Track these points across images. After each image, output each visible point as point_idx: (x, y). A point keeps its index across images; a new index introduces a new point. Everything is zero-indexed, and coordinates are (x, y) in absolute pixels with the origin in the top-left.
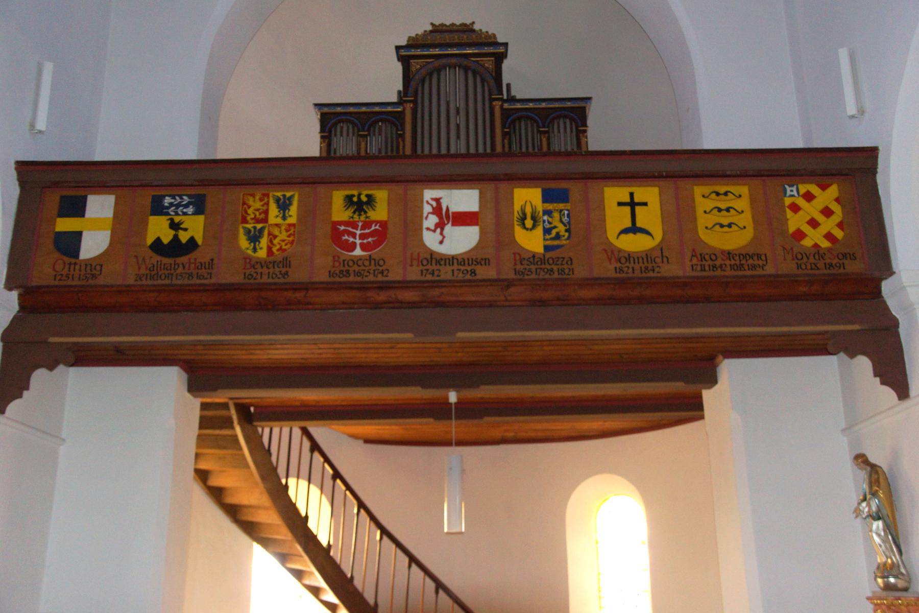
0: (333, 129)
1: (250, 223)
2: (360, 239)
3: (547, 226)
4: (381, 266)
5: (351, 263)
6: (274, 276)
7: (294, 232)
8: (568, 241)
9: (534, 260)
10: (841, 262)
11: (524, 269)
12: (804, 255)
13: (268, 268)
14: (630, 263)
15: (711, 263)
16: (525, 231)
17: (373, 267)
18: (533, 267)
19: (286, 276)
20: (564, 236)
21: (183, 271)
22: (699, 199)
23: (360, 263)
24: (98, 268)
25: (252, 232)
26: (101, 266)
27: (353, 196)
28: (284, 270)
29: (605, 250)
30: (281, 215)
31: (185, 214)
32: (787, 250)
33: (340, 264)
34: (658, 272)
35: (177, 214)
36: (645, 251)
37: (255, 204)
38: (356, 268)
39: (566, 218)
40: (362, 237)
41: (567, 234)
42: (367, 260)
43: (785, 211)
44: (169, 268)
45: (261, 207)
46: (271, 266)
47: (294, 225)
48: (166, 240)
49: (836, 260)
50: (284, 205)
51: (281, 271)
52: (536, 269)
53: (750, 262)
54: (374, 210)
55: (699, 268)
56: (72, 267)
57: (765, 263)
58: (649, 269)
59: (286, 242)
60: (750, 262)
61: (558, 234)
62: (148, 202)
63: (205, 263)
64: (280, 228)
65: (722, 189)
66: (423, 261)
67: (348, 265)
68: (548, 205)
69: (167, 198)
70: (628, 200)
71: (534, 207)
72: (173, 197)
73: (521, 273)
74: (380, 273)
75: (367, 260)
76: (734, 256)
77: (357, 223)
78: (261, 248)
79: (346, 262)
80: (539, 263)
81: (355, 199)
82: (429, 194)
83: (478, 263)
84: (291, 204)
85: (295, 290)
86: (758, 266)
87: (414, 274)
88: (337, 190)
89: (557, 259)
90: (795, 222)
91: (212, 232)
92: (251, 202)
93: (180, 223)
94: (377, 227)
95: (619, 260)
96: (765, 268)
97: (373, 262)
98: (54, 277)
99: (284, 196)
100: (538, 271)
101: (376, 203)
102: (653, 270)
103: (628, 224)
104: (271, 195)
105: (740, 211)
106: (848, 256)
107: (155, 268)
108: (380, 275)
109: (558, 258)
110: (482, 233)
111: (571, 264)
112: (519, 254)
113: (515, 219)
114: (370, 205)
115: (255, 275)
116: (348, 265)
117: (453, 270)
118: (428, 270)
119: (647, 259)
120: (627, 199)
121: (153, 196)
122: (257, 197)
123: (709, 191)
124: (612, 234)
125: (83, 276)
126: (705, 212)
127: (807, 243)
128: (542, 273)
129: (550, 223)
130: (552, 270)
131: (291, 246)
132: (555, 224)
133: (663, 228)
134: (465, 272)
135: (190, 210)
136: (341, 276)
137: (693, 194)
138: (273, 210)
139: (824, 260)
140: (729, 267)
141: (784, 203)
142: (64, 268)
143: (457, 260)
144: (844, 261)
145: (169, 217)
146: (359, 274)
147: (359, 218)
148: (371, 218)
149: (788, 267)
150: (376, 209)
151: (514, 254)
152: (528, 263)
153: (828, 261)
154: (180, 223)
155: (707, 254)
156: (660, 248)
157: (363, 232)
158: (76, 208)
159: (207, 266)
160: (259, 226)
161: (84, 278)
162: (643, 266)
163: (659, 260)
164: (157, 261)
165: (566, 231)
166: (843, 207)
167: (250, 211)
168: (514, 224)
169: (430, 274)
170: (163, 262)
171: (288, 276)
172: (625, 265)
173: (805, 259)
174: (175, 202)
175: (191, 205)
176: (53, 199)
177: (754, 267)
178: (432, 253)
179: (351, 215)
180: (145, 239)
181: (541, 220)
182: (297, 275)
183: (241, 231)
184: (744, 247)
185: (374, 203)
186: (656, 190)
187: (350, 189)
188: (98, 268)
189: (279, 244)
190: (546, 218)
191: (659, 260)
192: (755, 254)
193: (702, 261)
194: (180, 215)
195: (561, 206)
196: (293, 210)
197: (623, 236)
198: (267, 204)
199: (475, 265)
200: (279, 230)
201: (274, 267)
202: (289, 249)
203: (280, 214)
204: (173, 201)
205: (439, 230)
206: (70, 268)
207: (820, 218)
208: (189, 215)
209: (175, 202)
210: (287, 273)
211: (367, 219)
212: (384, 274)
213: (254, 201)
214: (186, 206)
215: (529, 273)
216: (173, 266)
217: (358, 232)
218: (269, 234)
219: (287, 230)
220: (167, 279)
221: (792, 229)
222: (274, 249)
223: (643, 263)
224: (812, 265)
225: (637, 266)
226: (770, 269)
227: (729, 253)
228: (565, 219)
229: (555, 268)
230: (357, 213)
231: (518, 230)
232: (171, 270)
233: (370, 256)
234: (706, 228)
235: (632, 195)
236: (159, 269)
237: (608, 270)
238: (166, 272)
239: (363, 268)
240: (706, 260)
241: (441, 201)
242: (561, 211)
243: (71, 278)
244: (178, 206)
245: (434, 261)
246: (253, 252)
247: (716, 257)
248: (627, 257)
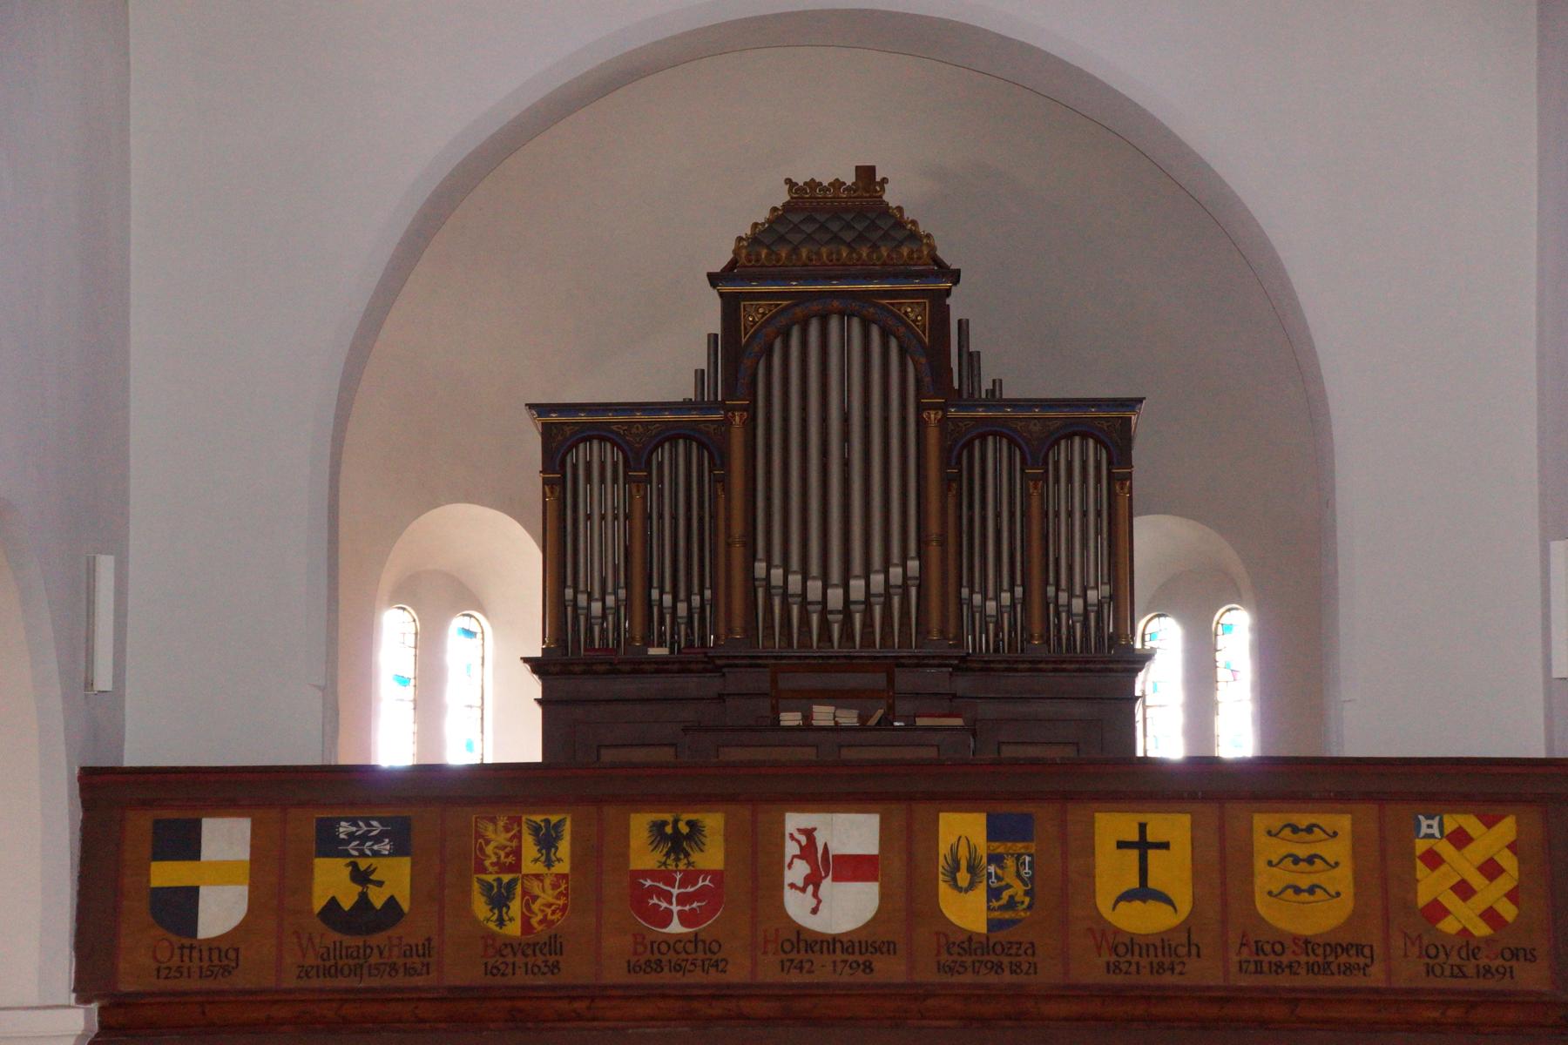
1: (491, 873)
2: (678, 904)
3: (994, 883)
4: (714, 953)
5: (664, 948)
6: (536, 970)
7: (566, 889)
8: (1028, 913)
9: (970, 944)
10: (1507, 964)
11: (953, 962)
12: (1441, 949)
13: (524, 954)
14: (1133, 954)
15: (1273, 958)
16: (956, 892)
17: (700, 955)
18: (968, 959)
19: (556, 971)
20: (1023, 903)
21: (381, 961)
22: (1260, 840)
23: (679, 946)
24: (232, 954)
25: (495, 890)
26: (237, 950)
27: (664, 823)
28: (552, 959)
29: (1090, 930)
30: (543, 859)
31: (376, 854)
32: (1410, 938)
33: (646, 947)
34: (1181, 973)
35: (363, 855)
36: (1160, 933)
37: (497, 837)
38: (672, 955)
39: (1027, 870)
40: (682, 900)
41: (1027, 900)
42: (690, 941)
43: (1414, 868)
44: (355, 954)
45: (509, 843)
46: (530, 952)
47: (564, 876)
48: (347, 904)
49: (1500, 962)
50: (547, 842)
51: (546, 962)
52: (974, 963)
53: (1343, 958)
54: (702, 851)
55: (1252, 967)
56: (186, 952)
57: (1368, 961)
58: (1166, 967)
59: (553, 907)
60: (1343, 958)
61: (1011, 897)
62: (310, 831)
63: (417, 946)
64: (542, 881)
65: (1304, 820)
66: (1119, 946)
67: (659, 951)
68: (997, 844)
69: (343, 824)
70: (1135, 837)
71: (972, 847)
72: (354, 823)
73: (947, 969)
74: (713, 966)
75: (690, 941)
76: (1316, 946)
77: (674, 874)
78: (511, 919)
79: (655, 946)
80: (979, 951)
81: (669, 830)
82: (795, 821)
83: (878, 950)
84: (559, 837)
85: (573, 999)
86: (1356, 966)
87: (770, 972)
88: (638, 812)
89: (1009, 946)
90: (1430, 886)
91: (431, 889)
92: (490, 834)
93: (370, 871)
94: (707, 882)
95: (1114, 949)
96: (1369, 970)
97: (700, 946)
98: (155, 973)
99: (547, 821)
100: (977, 964)
101: (705, 837)
102: (1173, 970)
103: (1134, 883)
104: (524, 819)
105: (1332, 863)
106: (1521, 954)
107: (332, 954)
108: (712, 970)
109: (1010, 943)
110: (884, 896)
111: (1034, 954)
112: (946, 936)
113: (940, 869)
114: (661, 838)
115: (502, 967)
116: (659, 951)
117: (834, 962)
118: (792, 961)
119: (1163, 948)
120: (1134, 836)
121: (320, 820)
122: (501, 824)
123: (1279, 824)
124: (1104, 904)
125: (207, 970)
126: (1270, 863)
127: (1449, 926)
128: (983, 971)
129: (999, 878)
130: (1000, 965)
131: (562, 916)
132: (1008, 880)
133: (1193, 893)
134: (854, 965)
135: (385, 847)
136: (648, 970)
137: (1250, 830)
138: (530, 849)
139: (1476, 959)
140: (1305, 967)
141: (1413, 848)
142: (172, 957)
143: (841, 942)
144: (1514, 963)
145: (348, 860)
146: (678, 968)
147: (677, 866)
148: (695, 864)
149: (1409, 973)
150: (706, 848)
151: (937, 934)
152: (961, 951)
153: (1483, 962)
154: (370, 871)
155: (1268, 942)
156: (1187, 927)
157: (682, 890)
158: (186, 845)
159: (421, 952)
160: (506, 878)
161: (209, 973)
162: (1155, 961)
163: (1183, 951)
164: (334, 942)
165: (1027, 893)
166: (1521, 862)
167: (489, 849)
168: (937, 879)
169: (795, 967)
170: (344, 944)
171: (559, 969)
172: (1125, 959)
173: (1442, 955)
174: (357, 831)
175: (386, 838)
176: (140, 824)
177: (1348, 969)
178: (800, 931)
179: (663, 859)
180: (310, 902)
181: (985, 872)
182: (576, 969)
183: (476, 886)
184: (1334, 931)
185: (701, 837)
186: (1186, 819)
187: (660, 811)
188: (232, 954)
189: (543, 911)
190: (992, 869)
191: (1183, 951)
192: (1352, 945)
193: (1258, 954)
194: (368, 856)
195: (1019, 847)
196: (564, 848)
197: (1123, 905)
198: (518, 836)
199: (871, 953)
200: (541, 884)
201: (535, 955)
202: (558, 920)
203: (542, 855)
204: (354, 829)
205: (810, 888)
206: (182, 956)
207: (1477, 880)
208: (384, 856)
209: (357, 831)
210: (556, 965)
211: (691, 868)
212: (720, 969)
213: (495, 831)
214: (378, 839)
215: (961, 970)
216: (361, 951)
217: (675, 891)
218: (525, 893)
219: (555, 886)
220: (352, 975)
221: (1423, 899)
222: (534, 921)
223: (1156, 956)
224: (1455, 968)
225: (1144, 962)
226: (1376, 976)
227: (1307, 942)
228: (1027, 871)
229: (1006, 960)
230: (672, 857)
231: (943, 888)
232: (358, 957)
233: (696, 934)
234: (1270, 893)
235: (1143, 827)
236: (338, 958)
237: (1092, 969)
238: (351, 962)
239: (684, 956)
240: (1266, 955)
241: (816, 834)
242: (1019, 856)
243: (185, 974)
244: (364, 838)
245: (802, 945)
246: (497, 926)
247: (1283, 948)
248: (1128, 943)
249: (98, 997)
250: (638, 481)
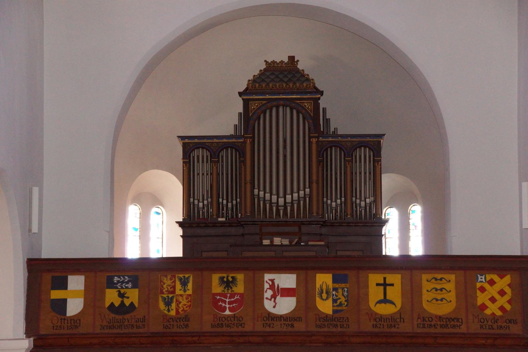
0: (325, 153)
1: (165, 294)
2: (228, 305)
3: (335, 297)
4: (240, 321)
5: (224, 319)
6: (180, 327)
7: (191, 299)
8: (346, 308)
9: (327, 318)
10: (508, 325)
11: (321, 324)
12: (485, 320)
13: (176, 321)
14: (381, 321)
15: (429, 323)
16: (322, 301)
17: (236, 322)
18: (326, 323)
19: (187, 327)
20: (344, 304)
21: (128, 324)
22: (424, 283)
23: (229, 319)
24: (78, 322)
25: (167, 300)
26: (80, 320)
27: (224, 277)
28: (186, 323)
29: (367, 313)
30: (183, 289)
31: (127, 288)
32: (475, 316)
33: (217, 319)
34: (398, 328)
35: (122, 288)
36: (391, 314)
37: (167, 282)
38: (226, 322)
39: (346, 293)
40: (230, 303)
41: (346, 303)
42: (232, 317)
43: (476, 292)
44: (120, 321)
45: (171, 284)
47: (190, 295)
48: (117, 304)
49: (505, 324)
50: (184, 283)
51: (184, 324)
52: (328, 324)
53: (452, 323)
54: (236, 287)
55: (422, 326)
56: (63, 321)
57: (461, 324)
58: (393, 326)
59: (186, 306)
60: (452, 323)
61: (341, 302)
62: (104, 280)
63: (140, 319)
64: (182, 297)
65: (439, 276)
67: (222, 320)
68: (336, 284)
69: (115, 277)
70: (382, 282)
71: (327, 285)
72: (119, 277)
73: (319, 326)
74: (240, 325)
75: (232, 317)
76: (443, 319)
77: (227, 294)
78: (172, 310)
79: (221, 319)
80: (330, 321)
81: (225, 279)
82: (268, 277)
83: (296, 320)
84: (188, 282)
85: (193, 336)
86: (457, 325)
87: (259, 327)
88: (215, 274)
89: (340, 319)
90: (482, 298)
91: (145, 299)
92: (165, 281)
93: (125, 293)
94: (238, 297)
95: (375, 320)
96: (461, 327)
97: (236, 319)
99: (184, 277)
100: (329, 325)
101: (238, 282)
102: (395, 327)
103: (382, 297)
104: (176, 276)
105: (449, 291)
106: (512, 321)
107: (112, 321)
108: (240, 327)
109: (340, 318)
110: (298, 302)
111: (348, 321)
112: (319, 315)
113: (317, 293)
115: (169, 326)
116: (222, 320)
117: (281, 324)
118: (267, 324)
119: (392, 319)
120: (382, 282)
121: (108, 276)
122: (169, 277)
123: (431, 278)
124: (372, 304)
125: (70, 327)
126: (428, 291)
127: (488, 312)
129: (336, 296)
130: (337, 325)
131: (189, 308)
132: (339, 296)
133: (402, 301)
134: (288, 325)
135: (130, 285)
136: (218, 327)
137: (421, 280)
138: (178, 286)
139: (497, 323)
140: (439, 326)
141: (476, 286)
142: (58, 322)
143: (283, 317)
144: (510, 324)
145: (117, 290)
146: (228, 326)
147: (228, 292)
148: (234, 291)
149: (475, 328)
150: (238, 286)
151: (316, 314)
152: (324, 320)
153: (499, 324)
154: (125, 293)
155: (427, 317)
156: (400, 312)
157: (230, 300)
158: (63, 285)
159: (142, 321)
160: (170, 296)
161: (70, 328)
162: (389, 324)
163: (398, 320)
164: (113, 317)
165: (346, 301)
166: (512, 290)
167: (165, 286)
168: (315, 296)
169: (268, 326)
170: (116, 318)
171: (188, 327)
172: (379, 323)
173: (486, 322)
174: (120, 280)
175: (130, 282)
176: (47, 278)
177: (454, 326)
178: (269, 313)
179: (223, 289)
180: (104, 304)
181: (332, 294)
182: (194, 327)
183: (160, 298)
184: (449, 314)
185: (236, 282)
186: (399, 276)
187: (222, 273)
188: (78, 322)
189: (183, 307)
190: (334, 293)
191: (398, 320)
192: (455, 318)
193: (423, 321)
194: (124, 288)
195: (343, 285)
196: (190, 286)
197: (378, 305)
198: (175, 282)
199: (293, 321)
200: (182, 298)
201: (180, 322)
202: (188, 310)
203: (183, 288)
204: (119, 279)
205: (273, 299)
206: (61, 322)
207: (497, 297)
208: (129, 288)
209: (120, 280)
210: (187, 325)
211: (233, 292)
212: (242, 326)
213: (167, 280)
214: (127, 283)
215: (324, 327)
216: (122, 320)
217: (227, 300)
218: (177, 301)
219: (187, 299)
220: (119, 329)
221: (479, 303)
222: (180, 310)
223: (389, 322)
224: (490, 326)
225: (385, 324)
226: (463, 329)
227: (440, 317)
228: (346, 293)
229: (339, 323)
230: (226, 289)
231: (318, 299)
232: (121, 322)
233: (234, 315)
234: (428, 301)
235: (385, 279)
236: (114, 323)
237: (368, 326)
238: (118, 324)
239: (230, 322)
240: (426, 322)
241: (275, 281)
242: (343, 288)
243: (62, 328)
244: (123, 282)
245: (270, 318)
246: (167, 312)
247: (432, 319)
248: (380, 318)
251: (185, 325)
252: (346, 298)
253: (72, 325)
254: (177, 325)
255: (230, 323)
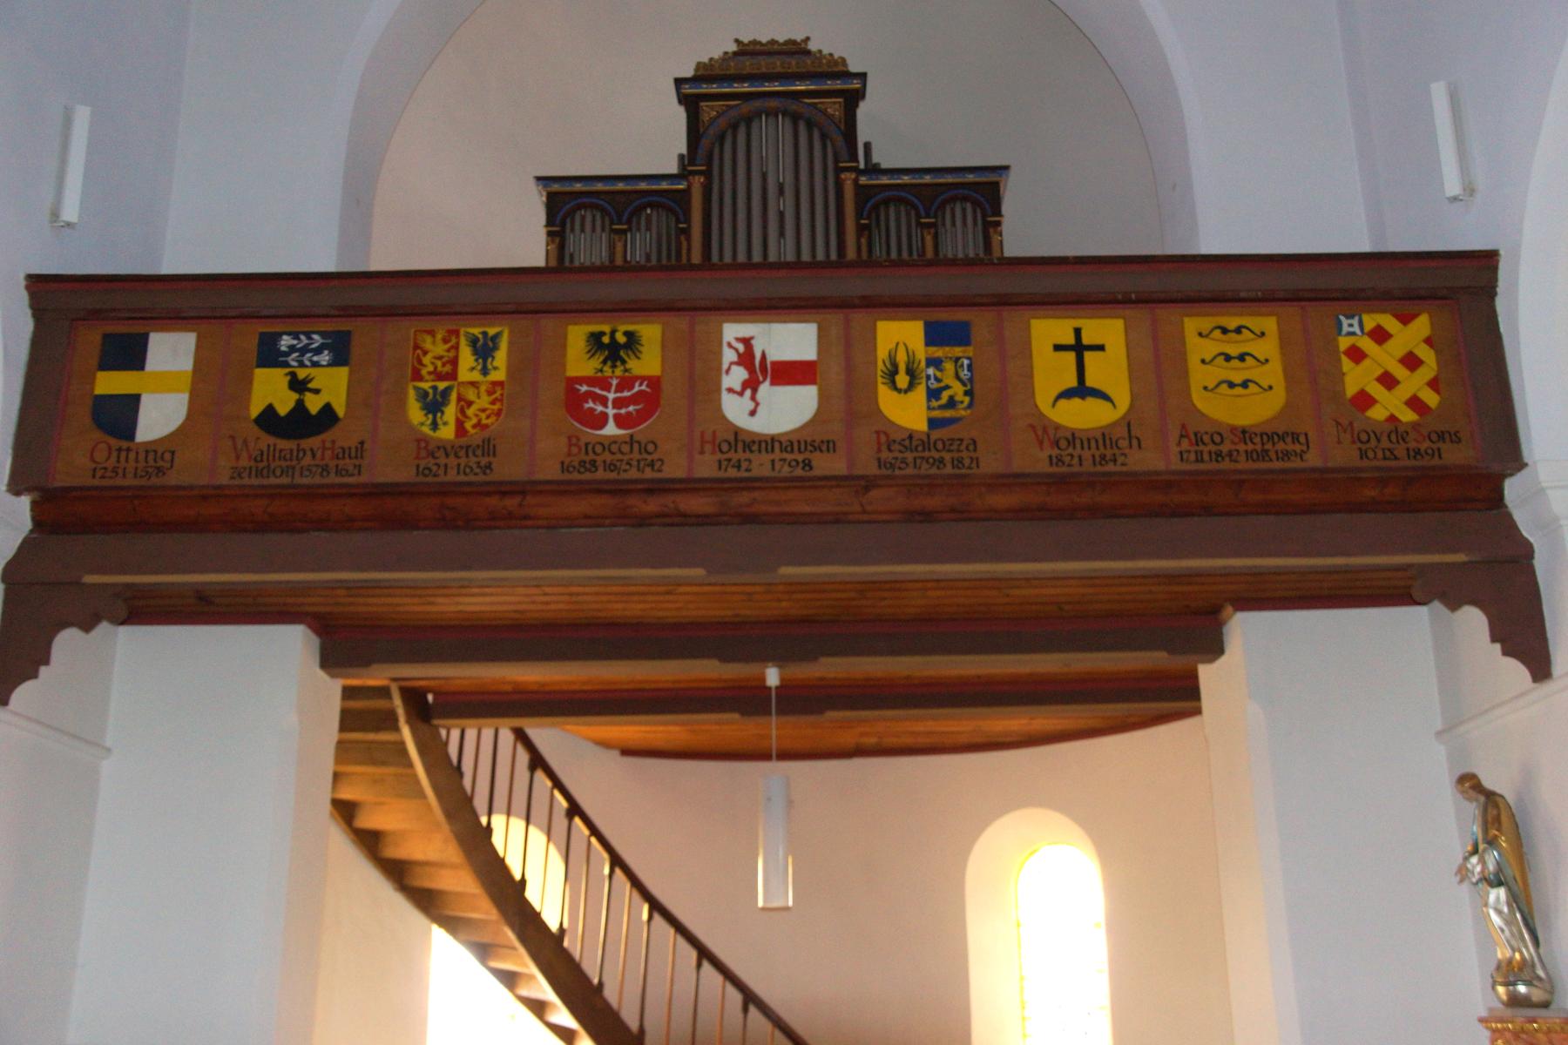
1: (427, 381)
2: (614, 407)
3: (934, 385)
4: (649, 453)
5: (599, 449)
6: (468, 470)
7: (502, 395)
8: (969, 411)
9: (911, 443)
10: (1435, 446)
11: (894, 458)
12: (1372, 435)
13: (457, 456)
14: (1074, 448)
15: (1213, 448)
16: (895, 393)
17: (636, 456)
18: (909, 456)
19: (488, 471)
20: (962, 402)
21: (313, 463)
22: (1192, 340)
23: (614, 448)
24: (168, 456)
25: (431, 396)
26: (173, 453)
27: (603, 334)
28: (484, 461)
29: (1033, 427)
30: (479, 367)
31: (315, 365)
32: (1342, 427)
33: (580, 449)
34: (1123, 464)
35: (302, 365)
36: (1101, 428)
37: (436, 348)
38: (608, 457)
39: (966, 372)
40: (618, 403)
41: (967, 399)
42: (626, 443)
43: (1339, 360)
44: (288, 456)
45: (445, 354)
47: (501, 384)
48: (283, 410)
49: (1427, 444)
50: (484, 350)
52: (915, 459)
53: (1280, 446)
54: (638, 358)
55: (1192, 457)
56: (123, 454)
57: (1305, 448)
58: (1107, 459)
59: (488, 412)
60: (1280, 446)
61: (951, 398)
62: (253, 344)
63: (350, 448)
64: (478, 388)
65: (1232, 323)
67: (594, 452)
68: (935, 349)
69: (285, 337)
70: (1071, 340)
71: (911, 353)
72: (296, 336)
73: (888, 465)
74: (648, 465)
75: (626, 443)
76: (1253, 436)
77: (610, 380)
78: (445, 424)
79: (590, 447)
80: (920, 448)
81: (606, 340)
82: (732, 331)
83: (816, 448)
84: (496, 348)
85: (504, 494)
86: (1293, 453)
87: (706, 467)
88: (576, 324)
89: (950, 442)
90: (1356, 378)
91: (362, 395)
92: (428, 344)
93: (307, 380)
94: (643, 387)
95: (1056, 444)
96: (1305, 457)
97: (636, 446)
99: (485, 334)
100: (918, 461)
101: (642, 345)
102: (1115, 461)
103: (1072, 382)
104: (462, 332)
105: (1262, 359)
106: (1447, 436)
107: (265, 457)
108: (648, 470)
109: (953, 440)
110: (823, 398)
111: (975, 450)
112: (885, 433)
113: (880, 373)
115: (434, 468)
116: (594, 452)
117: (773, 461)
118: (729, 460)
119: (1104, 441)
120: (1070, 339)
121: (262, 334)
122: (439, 336)
123: (1211, 326)
124: (1043, 399)
125: (142, 471)
126: (1203, 361)
127: (1377, 413)
129: (938, 380)
130: (941, 461)
131: (497, 420)
132: (946, 381)
133: (1131, 388)
134: (794, 463)
135: (325, 358)
136: (582, 470)
137: (1182, 331)
138: (467, 358)
139: (1406, 443)
140: (1244, 455)
141: (1337, 347)
142: (109, 458)
143: (780, 443)
144: (1440, 445)
145: (288, 370)
146: (612, 468)
147: (613, 372)
148: (632, 371)
149: (1344, 455)
150: (642, 356)
151: (878, 433)
152: (902, 448)
153: (1412, 445)
154: (307, 380)
155: (1207, 433)
156: (1127, 422)
157: (619, 395)
158: (130, 355)
159: (353, 454)
160: (442, 385)
161: (144, 474)
162: (1097, 454)
163: (1124, 443)
164: (269, 446)
165: (966, 393)
166: (1438, 353)
167: (427, 360)
168: (876, 382)
169: (733, 466)
170: (278, 447)
171: (491, 470)
172: (1066, 452)
173: (1373, 442)
174: (298, 344)
175: (326, 349)
176: (91, 339)
177: (1286, 455)
178: (737, 432)
179: (600, 367)
180: (247, 408)
181: (924, 375)
182: (508, 469)
183: (412, 394)
184: (1270, 421)
185: (638, 346)
186: (1119, 324)
187: (597, 323)
188: (168, 456)
189: (476, 415)
190: (931, 371)
191: (1124, 443)
192: (1287, 434)
193: (1198, 445)
194: (307, 366)
195: (958, 351)
196: (501, 357)
197: (1063, 403)
198: (456, 347)
199: (811, 451)
200: (476, 391)
201: (467, 456)
202: (492, 424)
203: (479, 364)
204: (295, 342)
205: (748, 393)
206: (119, 457)
207: (1399, 372)
208: (323, 366)
209: (298, 344)
210: (489, 466)
211: (627, 374)
212: (656, 468)
213: (434, 343)
214: (318, 351)
215: (903, 466)
216: (295, 454)
217: (611, 396)
218: (460, 399)
219: (490, 393)
220: (284, 476)
221: (1351, 390)
222: (468, 425)
223: (1098, 448)
224: (1386, 451)
225: (1087, 454)
226: (1313, 459)
227: (1244, 432)
228: (965, 374)
229: (947, 456)
230: (609, 363)
231: (884, 392)
232: (291, 460)
233: (632, 436)
234: (1205, 388)
235: (1078, 332)
236: (271, 458)
237: (1037, 460)
238: (284, 464)
239: (619, 456)
240: (1204, 444)
241: (753, 342)
242: (957, 359)
243: (121, 474)
244: (304, 351)
245: (740, 445)
246: (431, 429)
247: (1222, 438)
248: (1070, 438)
249: (28, 490)
250: (617, 232)
251: (483, 464)
252: (964, 384)
253: (150, 464)
254: (418, 466)
255: (618, 461)
